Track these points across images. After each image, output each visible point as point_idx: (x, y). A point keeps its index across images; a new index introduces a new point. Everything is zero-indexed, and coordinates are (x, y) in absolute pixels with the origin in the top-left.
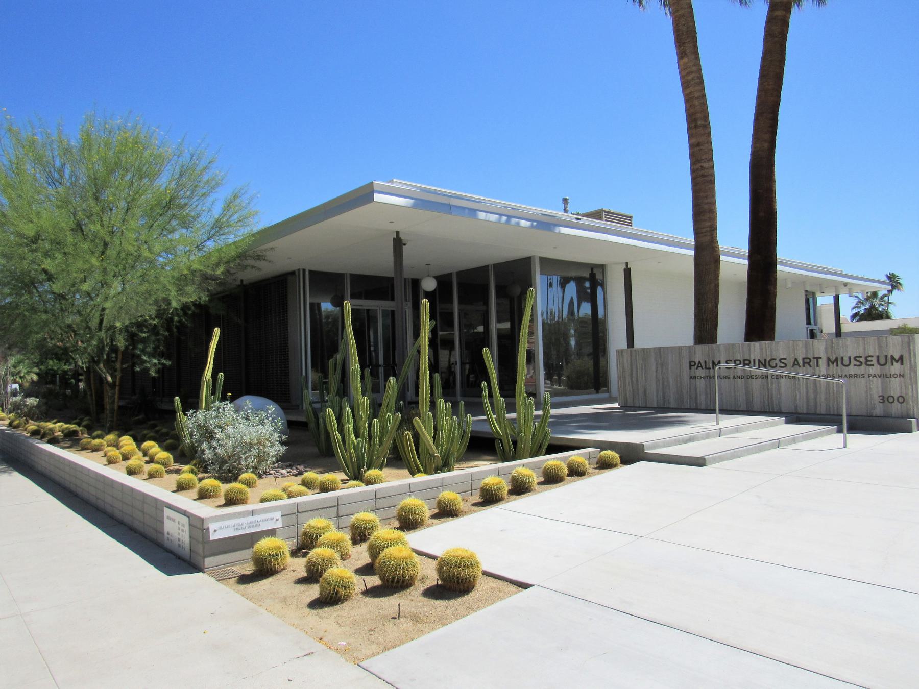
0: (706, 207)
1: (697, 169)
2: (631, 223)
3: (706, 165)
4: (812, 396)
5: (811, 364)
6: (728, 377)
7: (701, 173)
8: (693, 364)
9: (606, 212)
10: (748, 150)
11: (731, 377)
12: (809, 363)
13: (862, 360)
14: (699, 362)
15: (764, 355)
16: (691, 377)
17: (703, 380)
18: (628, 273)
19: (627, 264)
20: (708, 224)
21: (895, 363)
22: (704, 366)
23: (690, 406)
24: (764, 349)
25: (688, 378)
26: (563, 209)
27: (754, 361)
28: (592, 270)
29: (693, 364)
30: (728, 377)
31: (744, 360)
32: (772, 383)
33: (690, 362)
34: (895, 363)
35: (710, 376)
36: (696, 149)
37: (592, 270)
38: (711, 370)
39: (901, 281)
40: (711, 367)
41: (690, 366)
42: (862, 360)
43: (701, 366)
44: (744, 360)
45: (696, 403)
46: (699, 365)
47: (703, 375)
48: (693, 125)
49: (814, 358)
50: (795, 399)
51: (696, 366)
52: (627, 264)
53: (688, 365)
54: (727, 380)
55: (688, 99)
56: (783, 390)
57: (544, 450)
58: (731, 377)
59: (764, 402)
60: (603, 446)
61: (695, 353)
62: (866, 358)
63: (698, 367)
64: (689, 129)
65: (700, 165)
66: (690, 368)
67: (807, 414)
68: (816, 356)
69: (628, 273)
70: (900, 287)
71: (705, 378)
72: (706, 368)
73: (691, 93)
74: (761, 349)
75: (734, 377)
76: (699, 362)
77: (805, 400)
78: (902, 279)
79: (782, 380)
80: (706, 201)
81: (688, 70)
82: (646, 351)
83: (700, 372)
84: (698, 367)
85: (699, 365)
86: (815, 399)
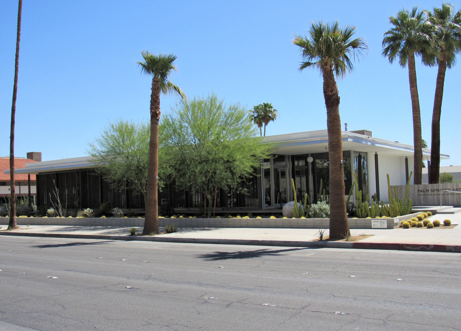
0: (419, 138)
1: (417, 125)
2: (371, 134)
3: (419, 124)
4: (458, 199)
5: (458, 190)
6: (432, 195)
7: (418, 126)
8: (419, 190)
9: (366, 131)
10: (431, 119)
11: (433, 194)
12: (438, 191)
13: (433, 190)
14: (421, 190)
15: (443, 187)
16: (418, 195)
17: (422, 196)
18: (376, 156)
19: (376, 152)
20: (420, 144)
21: (427, 192)
22: (423, 191)
23: (418, 204)
24: (443, 186)
25: (417, 195)
26: (345, 127)
27: (440, 189)
28: (360, 154)
29: (419, 190)
30: (432, 195)
31: (437, 189)
32: (446, 196)
33: (418, 190)
34: (427, 192)
35: (425, 195)
36: (416, 118)
37: (360, 154)
38: (426, 192)
39: (426, 144)
40: (425, 191)
41: (418, 191)
42: (433, 190)
43: (422, 191)
44: (437, 189)
45: (420, 203)
46: (421, 191)
47: (423, 194)
48: (415, 110)
49: (459, 189)
50: (453, 201)
51: (420, 191)
52: (376, 152)
53: (417, 191)
54: (431, 196)
55: (413, 101)
56: (449, 198)
57: (409, 213)
58: (433, 194)
59: (443, 202)
60: (426, 211)
61: (420, 187)
62: (434, 190)
63: (421, 191)
64: (413, 111)
65: (417, 124)
66: (418, 192)
67: (457, 205)
68: (460, 188)
69: (376, 156)
70: (426, 147)
71: (423, 195)
72: (424, 192)
73: (415, 100)
74: (442, 186)
75: (434, 195)
76: (421, 190)
77: (456, 201)
78: (427, 143)
79: (449, 196)
80: (419, 136)
81: (414, 92)
82: (391, 186)
83: (422, 193)
84: (421, 191)
85: (421, 191)
86: (459, 201)
